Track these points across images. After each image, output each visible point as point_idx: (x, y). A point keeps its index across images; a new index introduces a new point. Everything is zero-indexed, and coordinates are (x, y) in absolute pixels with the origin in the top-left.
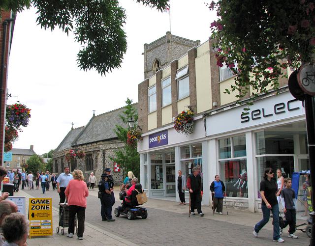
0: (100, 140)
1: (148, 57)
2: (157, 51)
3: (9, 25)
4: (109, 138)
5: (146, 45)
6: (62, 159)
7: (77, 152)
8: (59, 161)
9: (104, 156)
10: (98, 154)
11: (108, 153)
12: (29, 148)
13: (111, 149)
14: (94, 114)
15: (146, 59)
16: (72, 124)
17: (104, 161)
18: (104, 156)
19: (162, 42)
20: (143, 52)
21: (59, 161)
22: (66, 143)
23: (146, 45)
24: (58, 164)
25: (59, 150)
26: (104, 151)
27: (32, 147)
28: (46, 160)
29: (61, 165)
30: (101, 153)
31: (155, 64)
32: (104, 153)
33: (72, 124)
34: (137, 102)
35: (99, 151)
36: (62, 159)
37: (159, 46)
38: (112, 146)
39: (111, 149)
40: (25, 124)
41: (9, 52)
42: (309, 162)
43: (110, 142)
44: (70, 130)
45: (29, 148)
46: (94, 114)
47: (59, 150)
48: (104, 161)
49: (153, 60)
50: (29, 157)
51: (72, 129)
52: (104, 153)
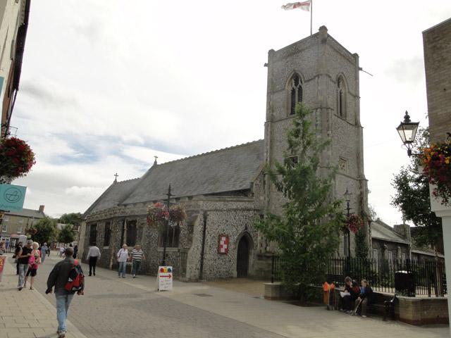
3: (13, 91)
4: (218, 191)
5: (271, 53)
7: (170, 208)
11: (212, 217)
12: (267, 68)
13: (216, 210)
14: (156, 162)
16: (116, 175)
17: (204, 232)
20: (267, 62)
22: (105, 201)
23: (271, 53)
24: (96, 232)
25: (94, 211)
26: (206, 212)
27: (42, 207)
28: (60, 226)
31: (291, 79)
32: (205, 217)
33: (116, 175)
34: (263, 138)
36: (108, 224)
38: (219, 205)
39: (216, 210)
41: (12, 84)
42: (125, 232)
43: (216, 198)
44: (112, 183)
46: (156, 162)
47: (94, 211)
48: (204, 232)
49: (288, 73)
50: (39, 221)
51: (115, 181)
52: (205, 217)
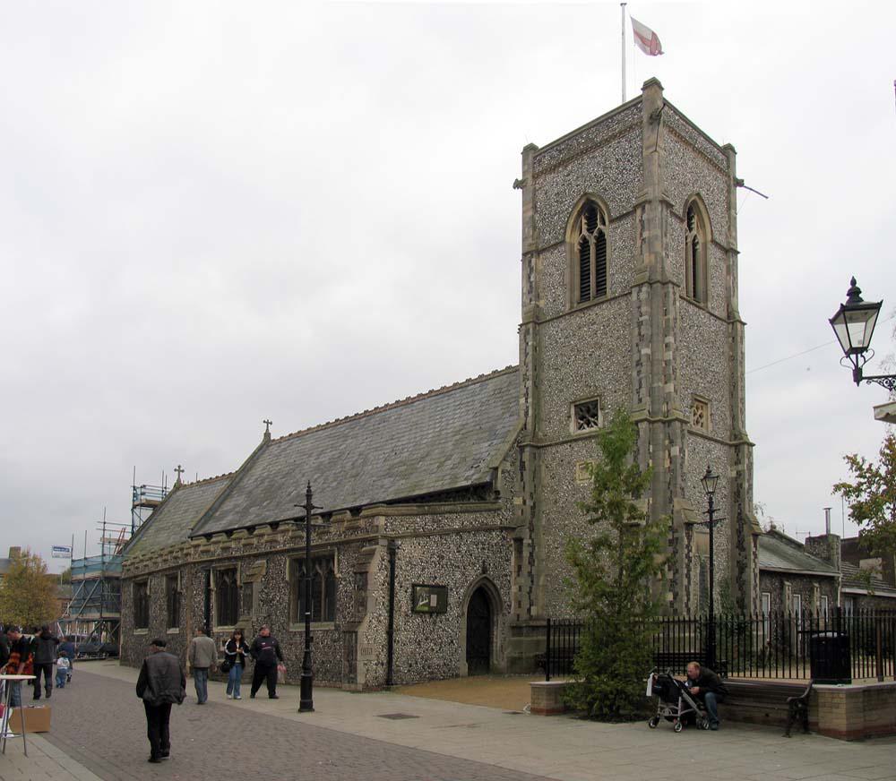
0: (219, 530)
1: (541, 196)
2: (590, 166)
5: (530, 150)
6: (172, 578)
8: (157, 586)
9: (392, 562)
10: (371, 554)
11: (407, 549)
14: (267, 435)
15: (531, 205)
16: (179, 470)
18: (392, 562)
19: (617, 128)
21: (157, 586)
23: (530, 150)
29: (163, 602)
30: (380, 551)
32: (392, 552)
33: (179, 470)
35: (373, 541)
36: (172, 578)
37: (598, 146)
40: (121, 665)
44: (259, 440)
45: (316, 695)
46: (267, 435)
49: (571, 202)
52: (392, 552)
